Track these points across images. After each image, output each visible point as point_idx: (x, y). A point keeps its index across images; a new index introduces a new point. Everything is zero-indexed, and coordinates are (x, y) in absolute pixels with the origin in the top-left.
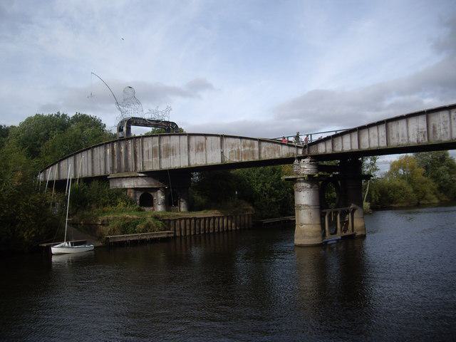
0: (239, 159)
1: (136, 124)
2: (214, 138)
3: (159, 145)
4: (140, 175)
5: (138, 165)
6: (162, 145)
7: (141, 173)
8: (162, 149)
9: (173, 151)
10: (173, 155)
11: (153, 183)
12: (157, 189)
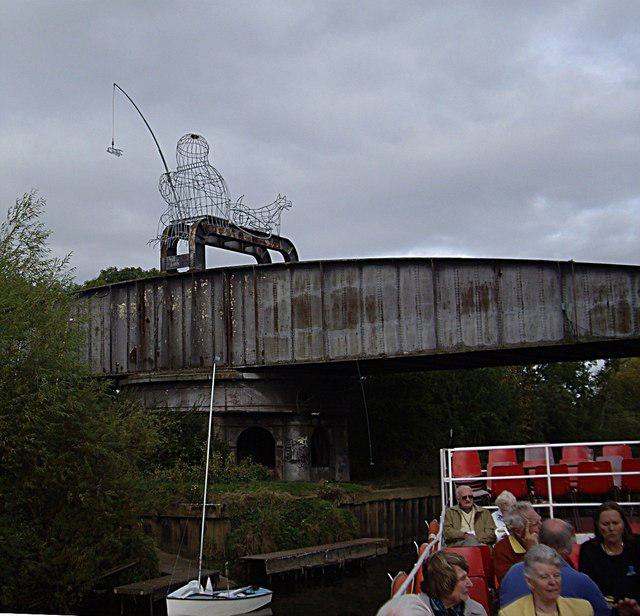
0: (625, 329)
1: (221, 242)
2: (525, 271)
3: (323, 293)
4: (246, 376)
5: (238, 348)
6: (329, 291)
7: (249, 370)
8: (329, 303)
9: (371, 307)
10: (372, 321)
11: (279, 401)
12: (290, 416)
